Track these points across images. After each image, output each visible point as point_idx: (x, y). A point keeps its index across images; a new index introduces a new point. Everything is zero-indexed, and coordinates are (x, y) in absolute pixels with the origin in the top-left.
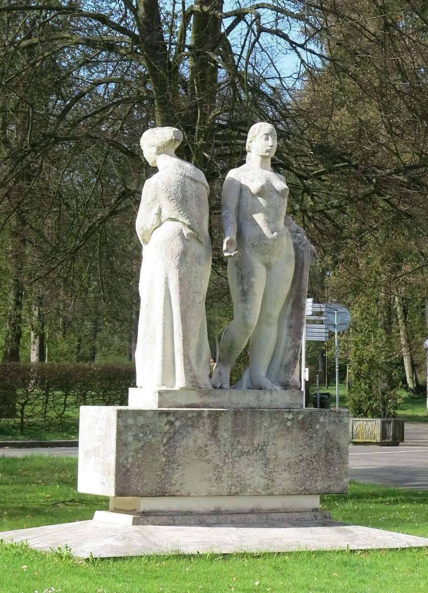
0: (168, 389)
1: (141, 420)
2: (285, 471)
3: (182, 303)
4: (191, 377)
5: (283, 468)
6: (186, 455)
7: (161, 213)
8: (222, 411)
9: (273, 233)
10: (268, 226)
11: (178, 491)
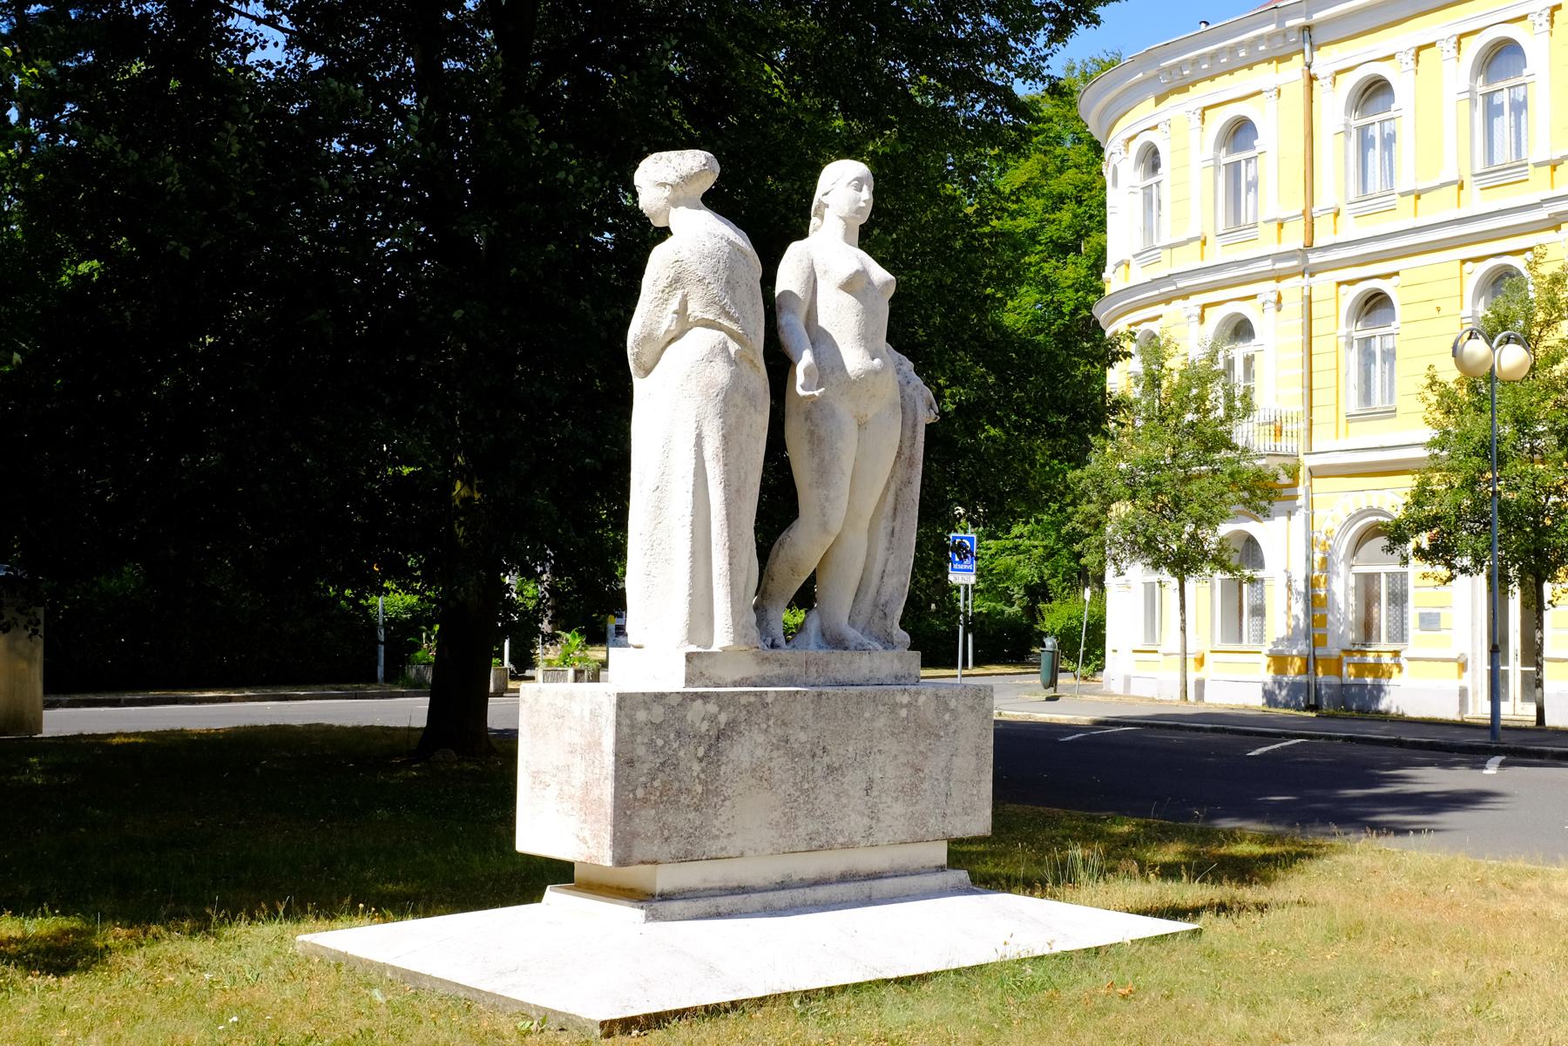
0: (700, 650)
1: (658, 712)
2: (897, 799)
3: (727, 485)
4: (743, 627)
5: (894, 795)
6: (738, 779)
7: (686, 309)
8: (797, 692)
9: (873, 359)
10: (865, 347)
11: (723, 849)
